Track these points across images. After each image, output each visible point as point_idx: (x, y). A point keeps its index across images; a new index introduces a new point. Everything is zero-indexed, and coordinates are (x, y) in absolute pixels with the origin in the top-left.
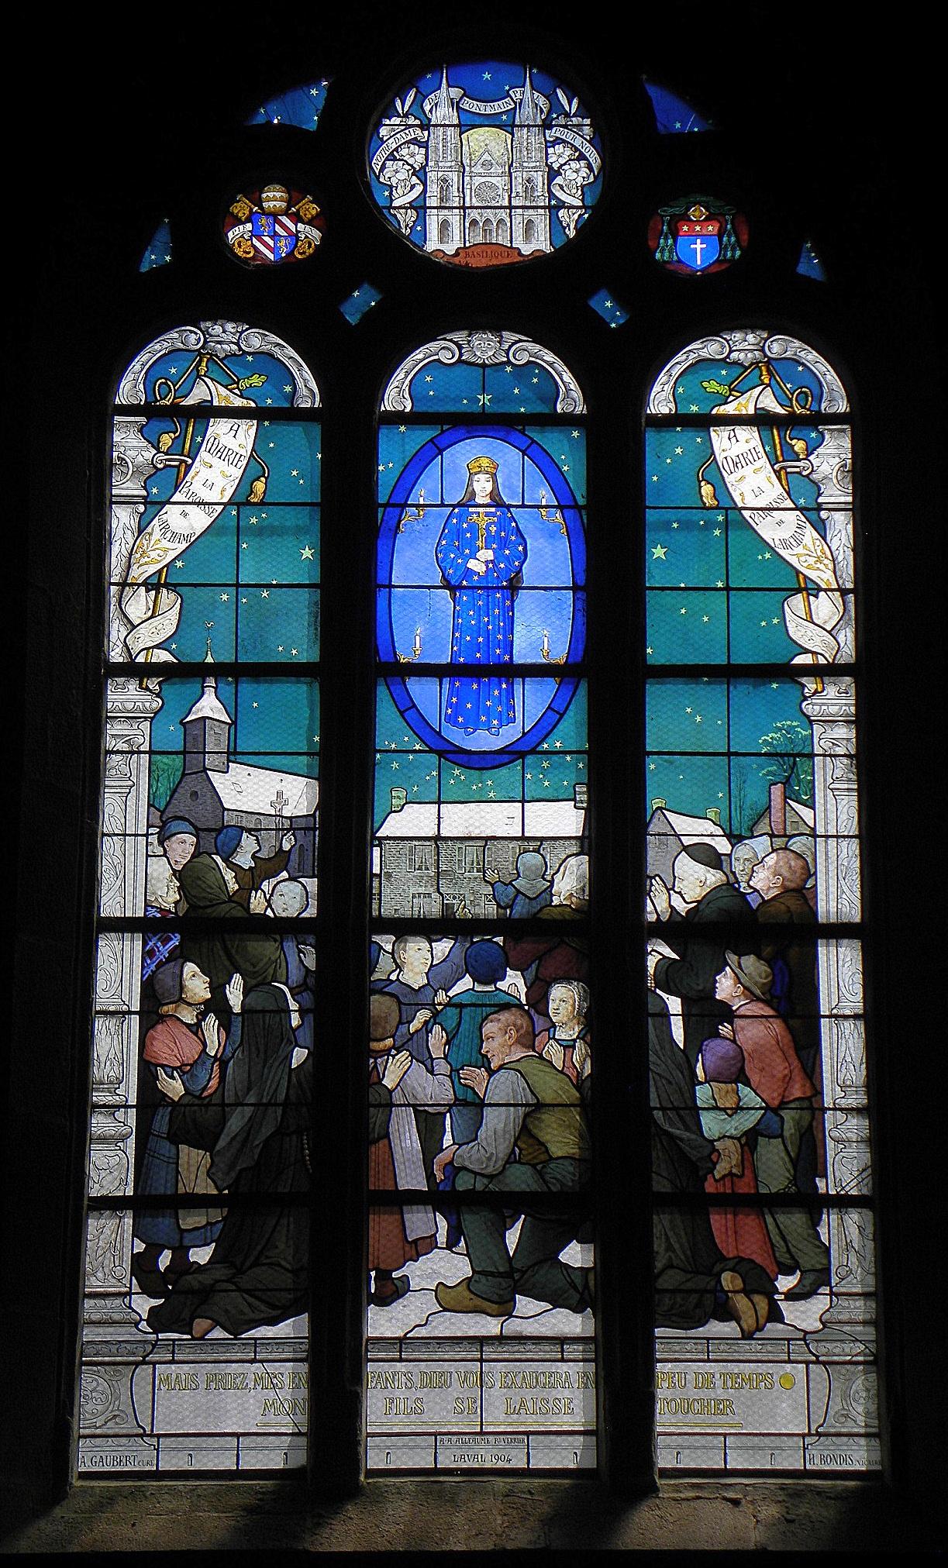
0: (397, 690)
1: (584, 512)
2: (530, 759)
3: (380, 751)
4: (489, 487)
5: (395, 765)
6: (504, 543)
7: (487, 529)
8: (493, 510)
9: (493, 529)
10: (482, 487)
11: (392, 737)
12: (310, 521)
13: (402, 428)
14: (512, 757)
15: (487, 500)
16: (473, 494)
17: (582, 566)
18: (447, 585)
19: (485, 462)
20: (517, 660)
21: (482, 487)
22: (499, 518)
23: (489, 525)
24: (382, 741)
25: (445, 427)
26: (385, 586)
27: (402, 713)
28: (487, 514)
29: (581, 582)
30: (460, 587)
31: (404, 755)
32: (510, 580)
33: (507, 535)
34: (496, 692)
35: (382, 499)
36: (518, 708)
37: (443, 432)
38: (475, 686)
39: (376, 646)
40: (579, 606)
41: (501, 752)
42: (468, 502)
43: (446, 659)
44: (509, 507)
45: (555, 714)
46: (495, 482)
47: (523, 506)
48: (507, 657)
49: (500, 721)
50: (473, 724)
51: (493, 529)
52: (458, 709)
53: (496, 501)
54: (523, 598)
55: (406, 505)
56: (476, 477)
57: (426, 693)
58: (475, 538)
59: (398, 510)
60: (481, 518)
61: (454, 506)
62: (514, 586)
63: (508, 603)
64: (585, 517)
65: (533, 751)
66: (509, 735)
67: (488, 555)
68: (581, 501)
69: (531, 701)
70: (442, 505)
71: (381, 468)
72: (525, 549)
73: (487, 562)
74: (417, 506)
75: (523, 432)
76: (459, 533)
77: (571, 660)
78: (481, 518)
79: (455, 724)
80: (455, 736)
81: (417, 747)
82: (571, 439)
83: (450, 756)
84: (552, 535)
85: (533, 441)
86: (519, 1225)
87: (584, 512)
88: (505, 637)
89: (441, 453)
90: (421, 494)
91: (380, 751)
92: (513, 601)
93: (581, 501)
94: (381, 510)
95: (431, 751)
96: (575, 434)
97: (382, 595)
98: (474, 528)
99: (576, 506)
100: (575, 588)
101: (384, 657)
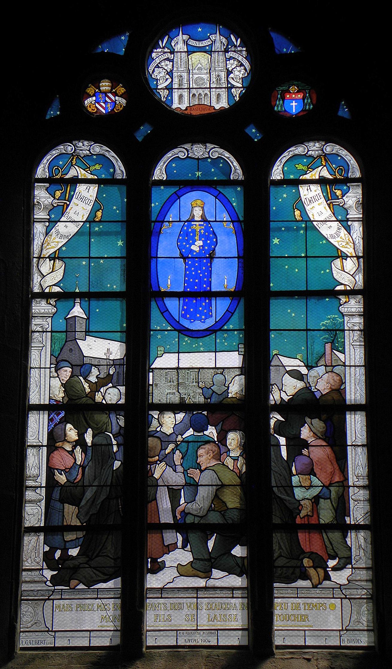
1: (242, 224)
2: (218, 333)
4: (201, 213)
5: (159, 337)
8: (202, 223)
9: (202, 231)
10: (198, 213)
13: (162, 187)
14: (211, 332)
17: (241, 248)
18: (183, 257)
20: (213, 290)
21: (198, 213)
23: (200, 230)
24: (154, 326)
25: (181, 187)
26: (154, 258)
27: (162, 313)
28: (200, 225)
29: (241, 254)
30: (188, 258)
32: (210, 254)
34: (204, 304)
35: (153, 219)
36: (214, 312)
37: (180, 189)
38: (194, 301)
40: (241, 265)
42: (191, 220)
43: (182, 290)
46: (203, 210)
47: (216, 221)
48: (208, 288)
49: (206, 316)
50: (193, 318)
51: (202, 231)
52: (187, 311)
53: (204, 219)
55: (163, 222)
56: (197, 209)
58: (195, 235)
59: (158, 220)
60: (197, 227)
61: (185, 222)
62: (212, 257)
63: (209, 264)
64: (243, 226)
65: (220, 330)
66: (210, 322)
67: (200, 243)
68: (241, 219)
69: (220, 307)
70: (180, 221)
71: (153, 205)
72: (217, 240)
73: (199, 247)
74: (169, 222)
76: (187, 234)
77: (237, 290)
78: (197, 227)
79: (185, 318)
80: (186, 323)
81: (169, 328)
83: (183, 332)
84: (228, 234)
85: (220, 192)
90: (170, 217)
92: (211, 264)
93: (241, 219)
94: (153, 224)
95: (175, 330)
96: (239, 189)
97: (153, 261)
98: (194, 231)
99: (239, 221)
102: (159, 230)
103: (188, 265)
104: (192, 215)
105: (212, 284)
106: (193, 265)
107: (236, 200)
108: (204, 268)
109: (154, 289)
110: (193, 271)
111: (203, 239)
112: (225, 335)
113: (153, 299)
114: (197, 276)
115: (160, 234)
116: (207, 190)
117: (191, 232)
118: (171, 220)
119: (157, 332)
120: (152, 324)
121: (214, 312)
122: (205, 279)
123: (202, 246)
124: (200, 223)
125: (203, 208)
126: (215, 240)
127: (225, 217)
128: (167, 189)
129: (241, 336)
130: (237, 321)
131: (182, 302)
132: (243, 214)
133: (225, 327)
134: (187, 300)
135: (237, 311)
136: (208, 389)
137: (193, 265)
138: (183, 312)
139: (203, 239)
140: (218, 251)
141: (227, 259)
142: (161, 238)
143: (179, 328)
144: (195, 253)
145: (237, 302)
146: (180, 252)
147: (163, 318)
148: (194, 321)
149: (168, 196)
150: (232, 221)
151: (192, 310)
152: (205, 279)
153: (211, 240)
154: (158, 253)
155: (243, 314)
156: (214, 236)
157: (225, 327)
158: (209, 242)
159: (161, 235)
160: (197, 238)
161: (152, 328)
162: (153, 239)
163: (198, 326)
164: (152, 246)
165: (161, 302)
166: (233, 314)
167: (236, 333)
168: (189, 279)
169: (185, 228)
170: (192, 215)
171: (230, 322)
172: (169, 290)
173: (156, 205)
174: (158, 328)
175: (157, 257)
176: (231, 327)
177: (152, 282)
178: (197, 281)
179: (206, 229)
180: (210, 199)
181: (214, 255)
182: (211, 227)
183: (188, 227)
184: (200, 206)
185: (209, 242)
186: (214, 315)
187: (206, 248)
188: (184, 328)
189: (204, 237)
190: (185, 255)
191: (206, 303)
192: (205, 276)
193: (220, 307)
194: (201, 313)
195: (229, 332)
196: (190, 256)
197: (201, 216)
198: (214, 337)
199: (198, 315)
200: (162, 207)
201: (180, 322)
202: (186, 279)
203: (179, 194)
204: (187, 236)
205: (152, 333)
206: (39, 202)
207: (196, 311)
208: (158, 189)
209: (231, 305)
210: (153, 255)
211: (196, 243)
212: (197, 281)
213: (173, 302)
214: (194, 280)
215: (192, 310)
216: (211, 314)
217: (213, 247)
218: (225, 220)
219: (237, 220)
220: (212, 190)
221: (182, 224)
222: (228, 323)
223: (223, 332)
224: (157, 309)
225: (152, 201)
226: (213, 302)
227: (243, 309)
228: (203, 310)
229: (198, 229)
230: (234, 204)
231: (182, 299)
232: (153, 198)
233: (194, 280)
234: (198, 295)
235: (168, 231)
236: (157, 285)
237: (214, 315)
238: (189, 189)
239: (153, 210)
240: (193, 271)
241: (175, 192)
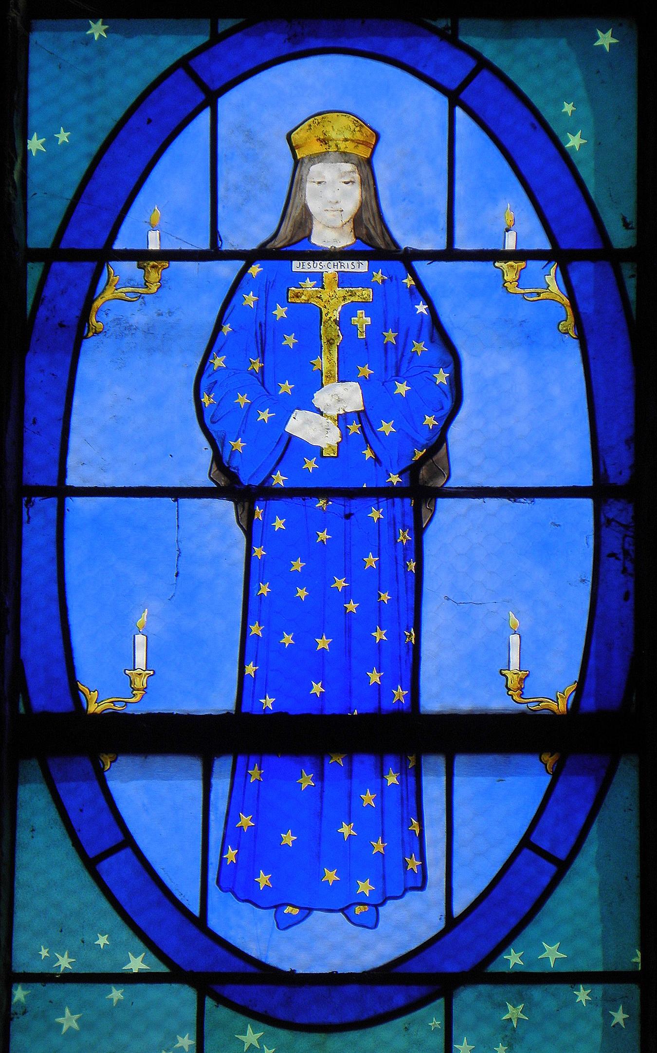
0: (79, 794)
1: (628, 270)
2: (467, 998)
3: (29, 978)
4: (351, 199)
5: (69, 1021)
6: (396, 363)
7: (344, 322)
8: (362, 267)
9: (362, 320)
10: (332, 202)
11: (60, 934)
12: (320, 713)
13: (97, 29)
14: (416, 992)
15: (345, 240)
16: (306, 220)
17: (620, 427)
18: (230, 485)
19: (340, 129)
20: (434, 701)
21: (332, 202)
22: (380, 291)
23: (349, 311)
24: (34, 951)
25: (224, 25)
26: (45, 492)
27: (91, 864)
28: (344, 280)
29: (620, 470)
30: (267, 492)
31: (89, 991)
32: (412, 471)
33: (403, 343)
34: (368, 798)
35: (40, 233)
36: (435, 852)
37: (216, 38)
38: (306, 781)
39: (19, 666)
40: (613, 542)
41: (387, 975)
42: (289, 247)
43: (221, 701)
44: (409, 257)
45: (537, 865)
46: (369, 182)
47: (450, 254)
48: (400, 694)
49: (381, 880)
50: (290, 903)
51: (362, 320)
52: (255, 848)
53: (373, 243)
54: (452, 526)
55: (106, 254)
56: (316, 170)
57: (164, 809)
58: (311, 346)
59: (70, 241)
60: (328, 291)
61: (249, 257)
62: (422, 487)
63: (404, 537)
64: (631, 285)
65: (480, 974)
66: (411, 923)
67: (349, 397)
68: (621, 238)
69: (484, 814)
70: (215, 253)
71: (35, 144)
72: (456, 381)
73: (343, 420)
74: (142, 256)
75: (451, 38)
76: (263, 337)
77: (589, 705)
78: (328, 291)
79: (250, 896)
80: (246, 928)
81: (136, 964)
82: (590, 56)
83: (228, 991)
84: (529, 339)
85: (483, 64)
86: (428, 21)
87: (628, 270)
88: (396, 637)
89: (211, 101)
90: (151, 224)
91: (29, 978)
92: (419, 532)
93: (621, 238)
94: (34, 271)
95: (176, 974)
96: (605, 40)
97: (38, 516)
98: (308, 319)
99: (604, 253)
100: (600, 491)
101: (43, 698)
102: (76, 312)
103: (271, 538)
104: (294, 212)
105: (427, 668)
106: (299, 541)
107: (586, 112)
108: (371, 561)
109: (40, 702)
110: (300, 579)
111: (365, 371)
112: (514, 1012)
113: (31, 768)
114: (323, 612)
115: (80, 337)
116: (395, 47)
117: (284, 327)
118: (154, 245)
119: (55, 991)
120: (20, 938)
121: (435, 852)
122: (379, 635)
123: (360, 416)
124: (349, 266)
125: (367, 166)
126: (442, 377)
127: (514, 223)
128: (136, 42)
129: (619, 1017)
130: (595, 912)
131: (221, 785)
132: (629, 207)
133: (513, 959)
134: (255, 774)
135: (591, 848)
136: (507, 686)
137: (299, 541)
138: (231, 855)
139: (365, 371)
140: (469, 453)
141: (524, 505)
142: (91, 366)
143: (202, 964)
144: (311, 465)
145: (591, 790)
146: (217, 458)
147: (93, 894)
148: (307, 911)
149: (137, 86)
150: (559, 255)
151: (288, 839)
152: (379, 635)
153: (420, 376)
154: (72, 460)
155: (634, 870)
156: (438, 352)
157: (513, 959)
158: (402, 389)
159: (87, 344)
160: (327, 361)
161: (22, 961)
162: (38, 369)
163: (326, 945)
164: (30, 411)
165: (88, 790)
166: (563, 867)
167: (582, 994)
168: (272, 634)
169: (250, 299)
170: (294, 212)
171: (544, 920)
172: (137, 705)
173: (55, 145)
174: (64, 963)
175: (62, 492)
176: (552, 955)
177: (26, 652)
178: (323, 643)
179: (383, 310)
180: (411, 109)
181: (436, 473)
182: (420, 291)
183: (270, 292)
184: (345, 157)
185: (402, 389)
186: (436, 873)
187: (387, 428)
188: (238, 966)
189: (377, 358)
190: (248, 477)
191: (382, 792)
192: (379, 615)
193: (484, 814)
194: (350, 859)
195: (537, 992)
196: (279, 479)
197: (357, 221)
198: (437, 1023)
199: (331, 876)
200: (97, 160)
201: (214, 922)
202: (255, 629)
203: (213, 70)
204: (252, 355)
205: (19, 994)
206: (250, 136)
207: (318, 846)
208: (68, 37)
209: (554, 807)
210: (38, 474)
211: (320, 398)
212: (323, 643)
213: (161, 787)
214: (305, 641)
215: (288, 839)
216: (413, 864)
217: (430, 421)
218: (510, 244)
219: (590, 244)
220: (428, 49)
221: (228, 270)
222: (531, 931)
223: (498, 991)
224: (59, 832)
225: (34, 120)
226: (433, 788)
227: (632, 836)
228: (361, 841)
229: (332, 302)
230: (574, 142)
231: (223, 767)
232: (34, 101)
233: (305, 641)
234: (338, 735)
235: (139, 318)
236: (60, 671)
237: (436, 873)
238: (278, 42)
239: (35, 178)
240: (300, 579)
241: (184, 63)
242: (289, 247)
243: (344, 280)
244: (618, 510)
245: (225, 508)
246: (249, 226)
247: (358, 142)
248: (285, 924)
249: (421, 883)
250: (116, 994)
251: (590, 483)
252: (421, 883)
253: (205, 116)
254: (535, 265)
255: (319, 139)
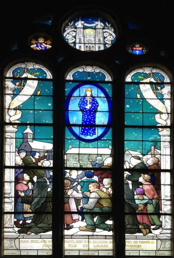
4: (90, 93)
6: (93, 104)
10: (89, 94)
21: (89, 94)
22: (92, 99)
28: (90, 98)
44: (94, 97)
52: (83, 132)
53: (92, 96)
62: (96, 111)
74: (74, 96)
76: (83, 102)
79: (83, 135)
80: (83, 137)
96: (109, 85)
119: (68, 140)
133: (102, 139)
161: (66, 138)
163: (88, 137)
174: (69, 138)
176: (105, 139)
193: (99, 132)
205: (66, 140)
211: (88, 105)
221: (81, 98)
242: (85, 96)
243: (90, 98)
244: (110, 113)
245: (81, 112)
246: (83, 95)
247: (147, 179)
248: (85, 136)
249: (95, 134)
250: (73, 140)
251: (162, 173)
252: (95, 134)
253: (147, 100)
254: (104, 98)
255: (33, 83)
